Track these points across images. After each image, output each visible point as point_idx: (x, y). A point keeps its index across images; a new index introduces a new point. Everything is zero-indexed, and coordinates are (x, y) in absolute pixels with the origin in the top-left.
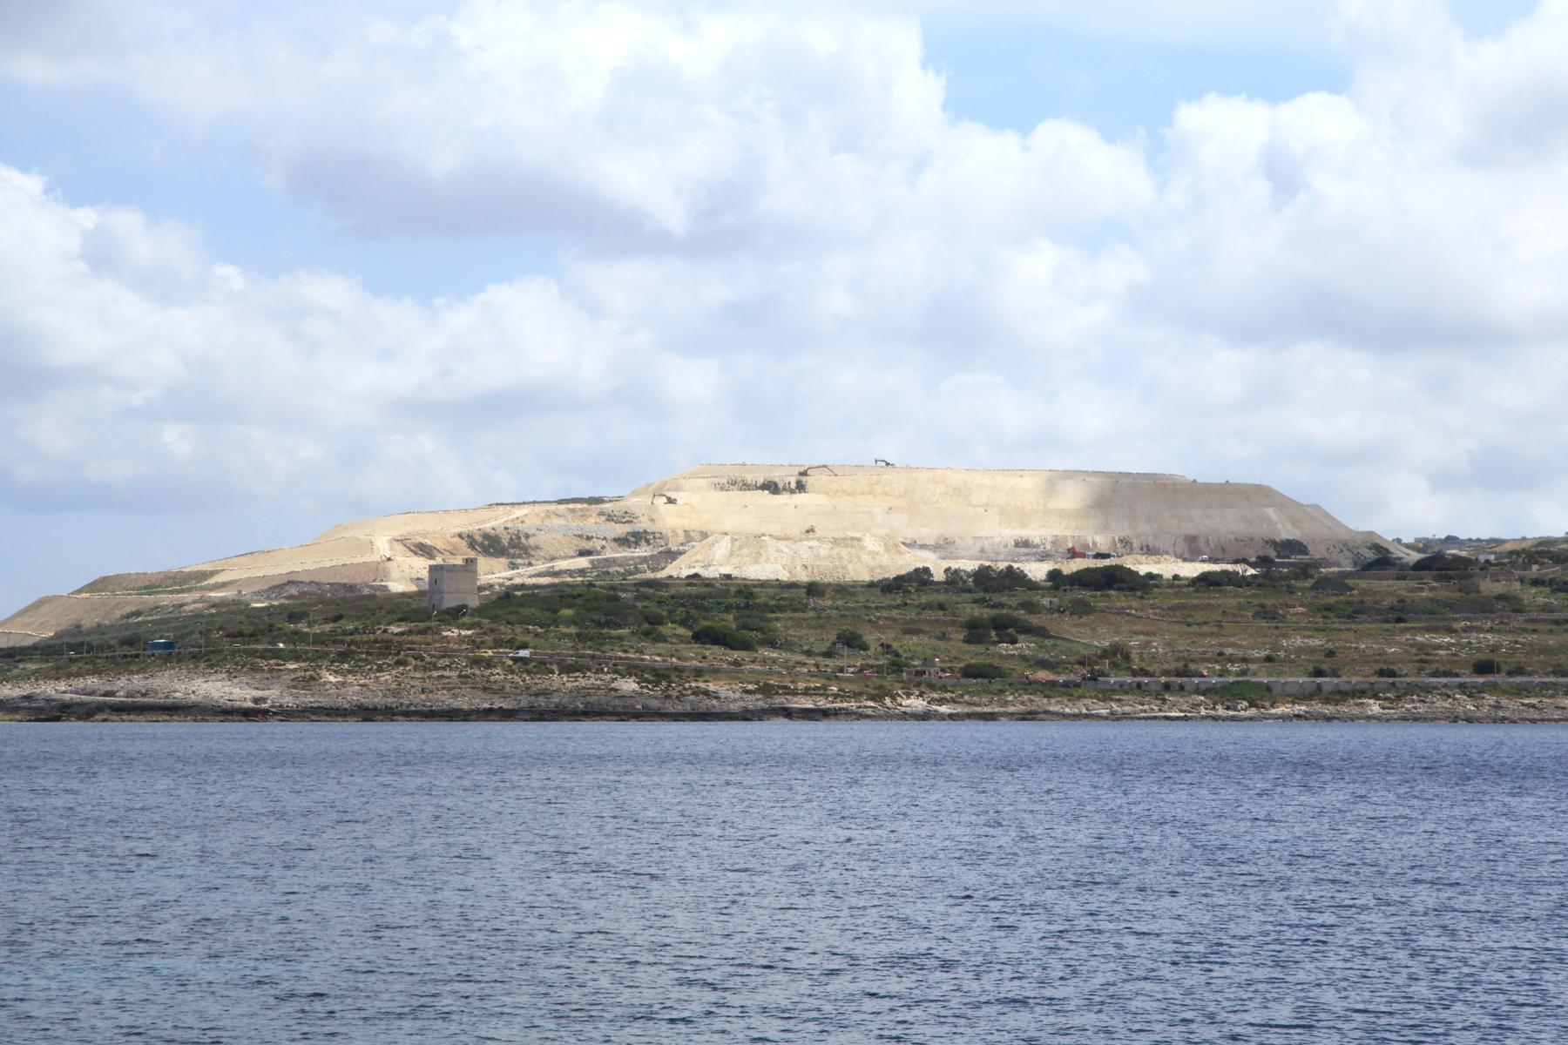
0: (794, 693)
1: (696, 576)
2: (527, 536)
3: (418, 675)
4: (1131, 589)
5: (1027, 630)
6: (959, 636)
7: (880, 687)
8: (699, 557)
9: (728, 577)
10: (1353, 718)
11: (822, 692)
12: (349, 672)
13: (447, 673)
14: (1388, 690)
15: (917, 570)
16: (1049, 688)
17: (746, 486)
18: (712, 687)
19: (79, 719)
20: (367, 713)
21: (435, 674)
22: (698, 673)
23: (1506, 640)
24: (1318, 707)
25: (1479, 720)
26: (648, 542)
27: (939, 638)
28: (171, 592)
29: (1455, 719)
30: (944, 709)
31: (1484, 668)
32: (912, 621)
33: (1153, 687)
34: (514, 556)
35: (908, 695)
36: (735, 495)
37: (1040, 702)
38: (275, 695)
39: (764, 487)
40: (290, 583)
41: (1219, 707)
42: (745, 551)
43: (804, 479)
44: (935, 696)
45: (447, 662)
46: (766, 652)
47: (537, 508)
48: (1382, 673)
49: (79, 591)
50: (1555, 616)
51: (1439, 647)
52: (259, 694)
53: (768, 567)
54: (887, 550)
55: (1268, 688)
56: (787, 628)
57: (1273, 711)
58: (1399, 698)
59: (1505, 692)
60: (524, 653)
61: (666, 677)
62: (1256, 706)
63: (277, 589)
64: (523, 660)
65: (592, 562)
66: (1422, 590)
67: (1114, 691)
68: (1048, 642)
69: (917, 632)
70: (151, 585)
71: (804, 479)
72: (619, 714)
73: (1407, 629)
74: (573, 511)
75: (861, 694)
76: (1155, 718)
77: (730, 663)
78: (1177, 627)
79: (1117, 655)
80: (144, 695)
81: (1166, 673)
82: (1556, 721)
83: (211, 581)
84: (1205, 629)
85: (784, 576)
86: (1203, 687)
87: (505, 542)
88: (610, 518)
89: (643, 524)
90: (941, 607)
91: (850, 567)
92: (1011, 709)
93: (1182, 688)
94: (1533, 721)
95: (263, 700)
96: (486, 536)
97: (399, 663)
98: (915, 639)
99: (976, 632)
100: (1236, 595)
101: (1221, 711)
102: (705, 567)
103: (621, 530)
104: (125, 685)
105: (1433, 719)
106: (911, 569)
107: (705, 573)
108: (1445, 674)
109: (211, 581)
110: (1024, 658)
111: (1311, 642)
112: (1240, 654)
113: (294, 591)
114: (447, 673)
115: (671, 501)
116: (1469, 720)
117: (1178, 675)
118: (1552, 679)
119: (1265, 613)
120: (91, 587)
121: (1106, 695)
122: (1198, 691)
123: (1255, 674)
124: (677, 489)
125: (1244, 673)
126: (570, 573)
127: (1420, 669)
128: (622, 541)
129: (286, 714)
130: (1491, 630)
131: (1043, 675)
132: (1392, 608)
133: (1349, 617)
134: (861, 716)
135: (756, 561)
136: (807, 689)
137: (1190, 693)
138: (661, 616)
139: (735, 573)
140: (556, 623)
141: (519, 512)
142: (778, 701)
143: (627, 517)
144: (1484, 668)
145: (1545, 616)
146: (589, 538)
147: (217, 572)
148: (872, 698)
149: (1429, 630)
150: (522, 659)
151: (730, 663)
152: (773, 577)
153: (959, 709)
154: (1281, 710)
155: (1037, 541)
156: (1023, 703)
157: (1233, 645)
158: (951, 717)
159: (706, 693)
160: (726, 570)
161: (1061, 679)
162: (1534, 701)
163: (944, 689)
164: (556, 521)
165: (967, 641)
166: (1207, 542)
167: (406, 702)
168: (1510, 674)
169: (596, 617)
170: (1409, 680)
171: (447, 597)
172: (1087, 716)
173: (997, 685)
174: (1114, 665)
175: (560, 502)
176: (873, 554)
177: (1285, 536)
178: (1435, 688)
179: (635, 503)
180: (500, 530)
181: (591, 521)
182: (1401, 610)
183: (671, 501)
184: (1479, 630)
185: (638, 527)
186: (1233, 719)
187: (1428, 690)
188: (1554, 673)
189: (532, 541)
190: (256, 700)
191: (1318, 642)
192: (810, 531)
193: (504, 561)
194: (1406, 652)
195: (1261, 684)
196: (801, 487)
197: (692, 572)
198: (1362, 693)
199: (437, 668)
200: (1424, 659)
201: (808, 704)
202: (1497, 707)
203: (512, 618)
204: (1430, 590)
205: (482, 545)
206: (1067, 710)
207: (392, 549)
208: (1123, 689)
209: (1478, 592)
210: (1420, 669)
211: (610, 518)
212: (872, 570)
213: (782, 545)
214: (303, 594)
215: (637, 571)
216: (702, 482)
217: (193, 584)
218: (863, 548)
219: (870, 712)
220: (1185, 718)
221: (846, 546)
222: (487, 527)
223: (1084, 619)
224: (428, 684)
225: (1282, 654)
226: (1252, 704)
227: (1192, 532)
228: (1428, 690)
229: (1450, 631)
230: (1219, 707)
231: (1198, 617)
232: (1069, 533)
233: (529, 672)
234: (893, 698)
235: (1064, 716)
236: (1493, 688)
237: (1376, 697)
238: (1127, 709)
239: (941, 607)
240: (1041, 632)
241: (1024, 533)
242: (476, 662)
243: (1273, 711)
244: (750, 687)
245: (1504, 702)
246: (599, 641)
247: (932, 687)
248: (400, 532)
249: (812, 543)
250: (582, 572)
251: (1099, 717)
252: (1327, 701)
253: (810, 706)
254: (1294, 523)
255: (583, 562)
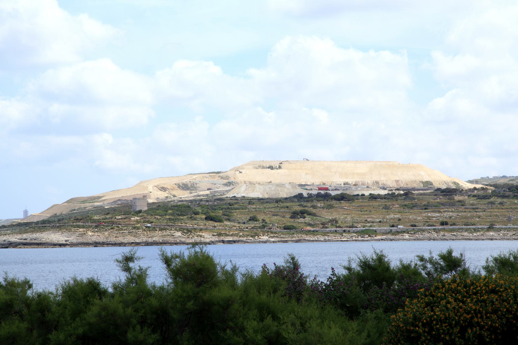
0: (228, 235)
1: (234, 197)
2: (196, 184)
3: (116, 232)
4: (349, 200)
5: (310, 214)
6: (288, 216)
7: (256, 233)
8: (236, 191)
9: (244, 197)
10: (399, 240)
11: (236, 235)
12: (96, 231)
13: (125, 231)
14: (412, 231)
15: (299, 194)
16: (308, 232)
17: (263, 167)
18: (203, 234)
19: (13, 247)
20: (96, 244)
21: (121, 232)
22: (201, 230)
23: (455, 214)
24: (390, 236)
25: (437, 240)
26: (233, 185)
27: (283, 217)
28: (89, 203)
29: (430, 239)
30: (273, 240)
31: (442, 224)
32: (277, 212)
33: (340, 231)
34: (192, 190)
35: (263, 235)
36: (260, 170)
37: (304, 237)
38: (73, 239)
39: (269, 168)
40: (119, 200)
41: (359, 237)
42: (250, 189)
43: (281, 165)
44: (272, 235)
45: (125, 228)
46: (227, 223)
47: (200, 175)
48: (412, 226)
49: (65, 202)
50: (474, 207)
51: (434, 217)
52: (67, 239)
53: (256, 194)
54: (293, 188)
55: (376, 231)
56: (237, 215)
57: (375, 238)
58: (415, 233)
59: (447, 231)
60: (149, 225)
61: (191, 232)
62: (370, 236)
63: (115, 202)
64: (149, 227)
65: (210, 192)
66: (437, 199)
67: (328, 233)
68: (315, 218)
69: (277, 215)
70: (85, 200)
71: (281, 165)
72: (170, 243)
73: (427, 212)
74: (211, 176)
75: (248, 235)
76: (338, 241)
77: (213, 226)
78: (357, 212)
79: (334, 222)
80: (35, 240)
81: (347, 227)
82: (460, 239)
83: (103, 199)
84: (366, 212)
85: (261, 196)
86: (356, 231)
87: (189, 186)
88: (222, 178)
89: (232, 180)
90: (287, 207)
91: (281, 193)
92: (294, 239)
93: (349, 231)
94: (453, 240)
95: (68, 241)
96: (183, 184)
97: (112, 229)
98: (276, 217)
99: (295, 215)
100: (380, 202)
101: (360, 238)
102: (237, 194)
103: (225, 181)
104: (28, 236)
105: (423, 240)
106: (297, 194)
107: (237, 196)
108: (431, 226)
109: (103, 199)
110: (305, 223)
111: (396, 216)
112: (372, 220)
113: (119, 202)
114: (125, 231)
115: (240, 172)
116: (434, 240)
117: (350, 227)
118: (464, 227)
119: (386, 208)
120: (68, 202)
121: (325, 234)
122: (354, 232)
123: (374, 226)
124: (243, 169)
125: (371, 226)
126: (203, 195)
127: (424, 224)
128: (226, 185)
129: (72, 245)
130: (452, 211)
131: (309, 228)
132: (424, 205)
133: (411, 208)
134: (245, 242)
135: (253, 192)
136: (232, 234)
137: (351, 233)
138: (199, 212)
139: (246, 196)
140: (166, 215)
141: (194, 177)
142: (222, 238)
143: (227, 178)
144: (442, 224)
145: (471, 207)
146: (215, 184)
147: (102, 197)
148: (252, 237)
149: (433, 212)
150: (148, 227)
151: (213, 226)
152: (257, 196)
153: (278, 239)
154: (379, 237)
155: (350, 183)
156: (298, 237)
157: (372, 217)
158: (273, 242)
159: (201, 236)
160: (243, 195)
161: (312, 229)
162: (455, 233)
163: (276, 233)
164: (205, 179)
165: (291, 218)
166: (402, 182)
167: (109, 241)
168: (451, 225)
169: (177, 213)
170: (418, 228)
171: (138, 207)
172: (316, 241)
173: (292, 231)
174: (332, 225)
175: (208, 173)
176: (288, 189)
177: (426, 180)
178: (426, 230)
179: (230, 174)
180: (188, 182)
181: (216, 179)
182: (427, 206)
183: (240, 172)
184: (449, 211)
185: (230, 180)
186: (363, 241)
187: (424, 231)
188: (465, 225)
189: (198, 185)
190: (66, 241)
191: (398, 216)
192: (271, 182)
193: (188, 191)
194: (424, 219)
195: (373, 230)
196: (280, 167)
197: (233, 195)
198: (404, 232)
199: (122, 230)
200: (428, 223)
201: (231, 239)
202: (444, 235)
203: (153, 214)
204: (441, 199)
205: (182, 187)
206: (311, 239)
207: (153, 189)
208: (331, 232)
209: (454, 199)
210: (424, 224)
211: (222, 178)
212: (287, 194)
213: (261, 187)
214: (122, 203)
215: (224, 194)
216: (250, 167)
217: (96, 200)
218: (285, 187)
219: (249, 241)
220: (347, 241)
221: (280, 187)
222: (184, 181)
223: (330, 210)
224: (118, 235)
225: (385, 220)
226: (369, 236)
227: (398, 179)
228: (424, 231)
229: (440, 212)
230: (359, 237)
231: (365, 209)
232: (360, 180)
233: (149, 231)
234: (258, 236)
235: (309, 241)
236: (444, 230)
237: (408, 233)
238: (330, 238)
239: (287, 207)
240: (314, 215)
241: (346, 180)
242: (134, 228)
243: (375, 238)
244: (215, 234)
245: (446, 234)
246: (174, 220)
247: (272, 233)
248: (156, 184)
249: (270, 186)
250: (207, 195)
251: (320, 241)
252: (393, 234)
253: (231, 239)
254: (429, 176)
255: (208, 192)
